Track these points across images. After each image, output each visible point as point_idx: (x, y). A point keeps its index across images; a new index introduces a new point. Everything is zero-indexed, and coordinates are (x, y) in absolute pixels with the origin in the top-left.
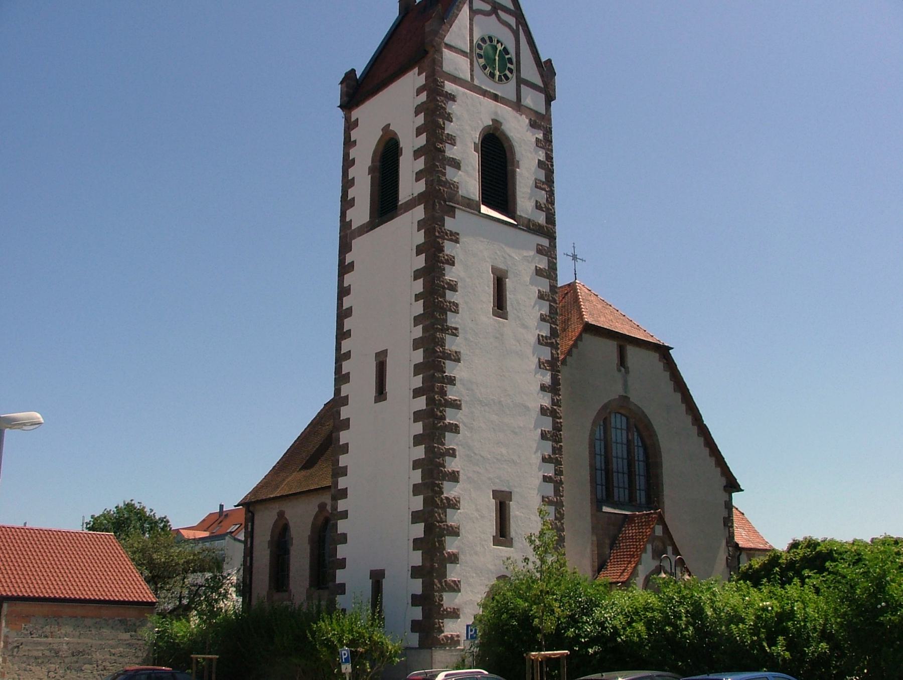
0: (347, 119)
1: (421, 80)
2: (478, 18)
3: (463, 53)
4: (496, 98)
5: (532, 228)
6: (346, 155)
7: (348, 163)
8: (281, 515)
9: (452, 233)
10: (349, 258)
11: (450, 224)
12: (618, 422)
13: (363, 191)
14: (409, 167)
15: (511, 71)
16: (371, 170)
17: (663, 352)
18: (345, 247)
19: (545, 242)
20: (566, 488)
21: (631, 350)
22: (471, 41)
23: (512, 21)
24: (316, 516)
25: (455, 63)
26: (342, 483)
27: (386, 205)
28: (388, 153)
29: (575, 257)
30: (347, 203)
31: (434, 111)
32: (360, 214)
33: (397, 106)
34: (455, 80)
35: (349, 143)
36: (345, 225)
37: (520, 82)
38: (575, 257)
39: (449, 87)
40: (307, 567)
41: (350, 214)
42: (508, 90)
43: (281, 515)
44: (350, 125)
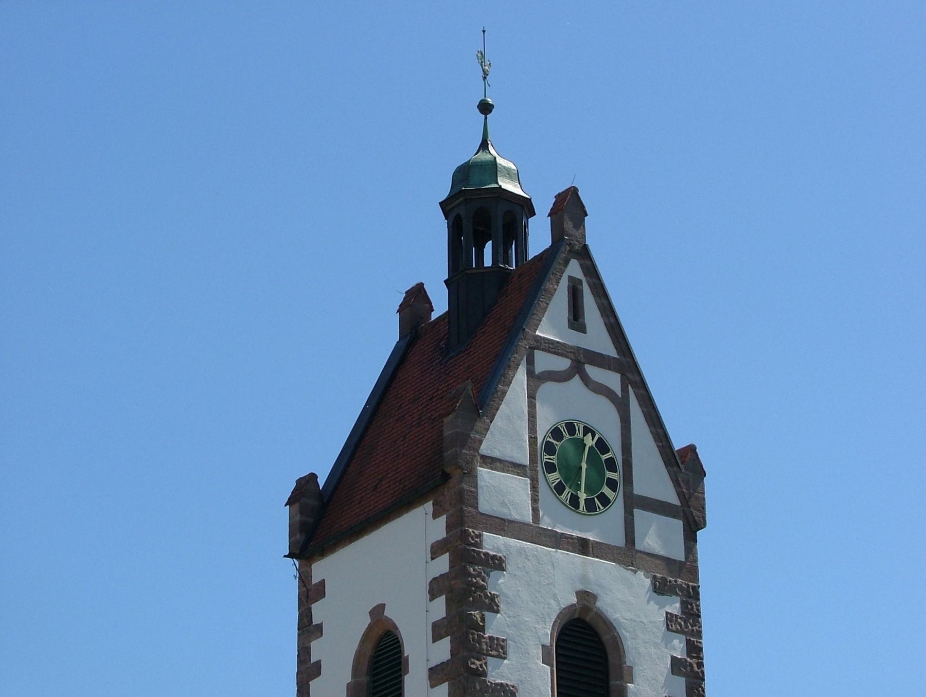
0: (304, 578)
1: (438, 529)
2: (547, 389)
4: (583, 547)
6: (304, 653)
15: (612, 485)
22: (533, 440)
23: (613, 380)
25: (502, 492)
31: (465, 590)
33: (392, 567)
34: (503, 526)
35: (308, 629)
37: (633, 503)
39: (492, 543)
42: (605, 527)
44: (310, 593)
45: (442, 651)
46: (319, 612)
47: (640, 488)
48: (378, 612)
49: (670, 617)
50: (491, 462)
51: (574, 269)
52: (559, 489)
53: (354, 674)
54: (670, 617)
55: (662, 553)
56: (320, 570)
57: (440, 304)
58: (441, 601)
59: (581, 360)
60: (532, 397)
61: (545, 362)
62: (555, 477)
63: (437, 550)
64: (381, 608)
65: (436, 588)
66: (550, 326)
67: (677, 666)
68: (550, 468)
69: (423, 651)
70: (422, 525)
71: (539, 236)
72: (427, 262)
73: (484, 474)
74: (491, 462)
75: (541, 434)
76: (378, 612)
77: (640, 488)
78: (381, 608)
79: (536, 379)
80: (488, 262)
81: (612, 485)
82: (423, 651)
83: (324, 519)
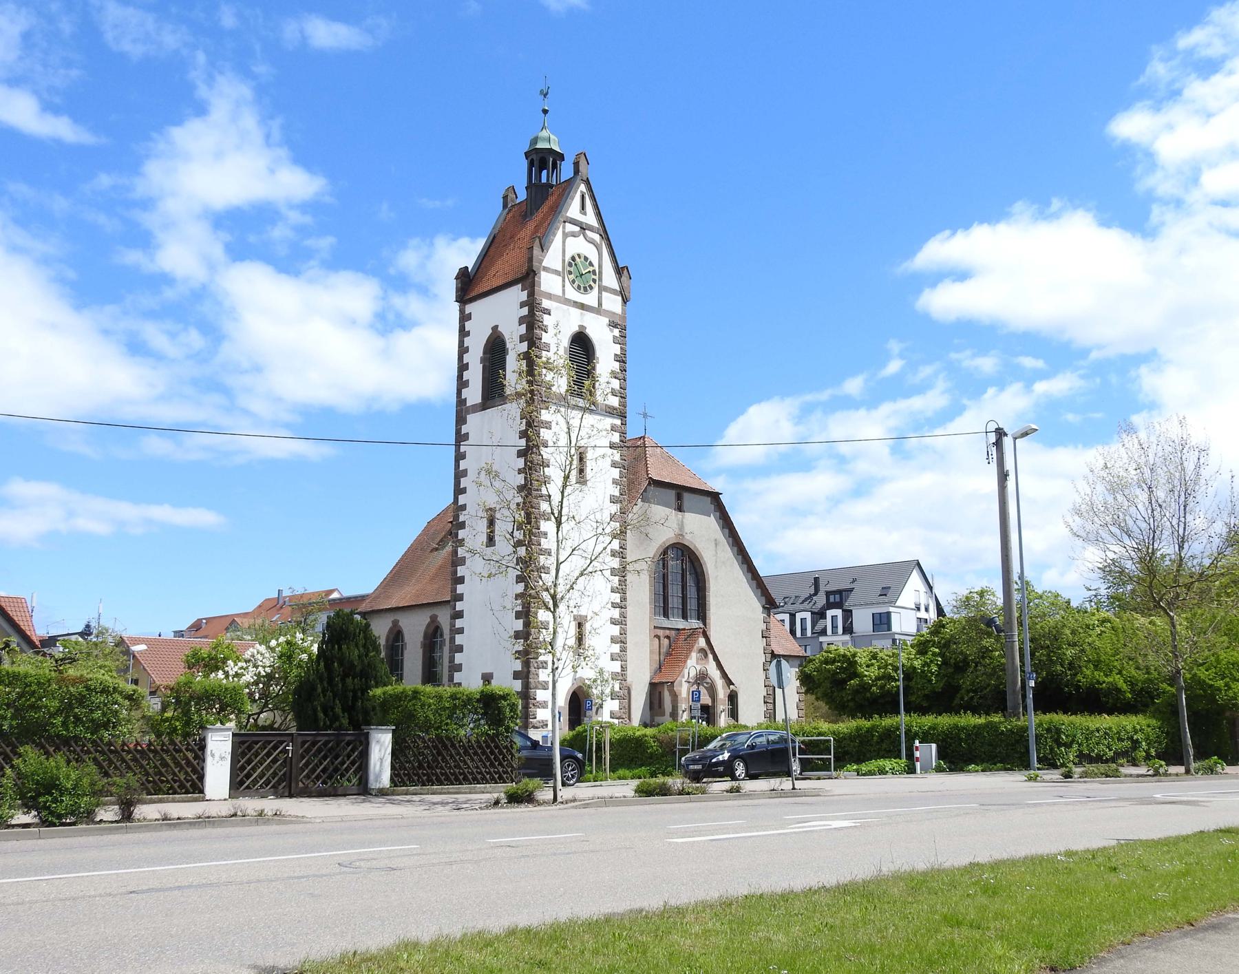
0: (462, 311)
1: (524, 296)
2: (570, 240)
3: (556, 272)
4: (582, 307)
5: (610, 412)
6: (461, 343)
7: (463, 350)
8: (395, 623)
9: (547, 422)
10: (464, 429)
11: (545, 415)
12: (674, 564)
13: (475, 375)
14: (513, 364)
15: (594, 281)
16: (483, 360)
17: (715, 497)
18: (461, 420)
19: (618, 422)
20: (630, 612)
21: (686, 496)
22: (564, 261)
23: (597, 237)
24: (429, 625)
25: (548, 283)
26: (459, 606)
27: (493, 392)
28: (495, 349)
29: (645, 416)
30: (462, 384)
31: (532, 322)
32: (474, 394)
33: (501, 311)
34: (550, 296)
35: (463, 333)
36: (461, 402)
37: (602, 289)
38: (645, 416)
39: (546, 303)
40: (420, 668)
41: (465, 393)
42: (591, 299)
43: (395, 623)
44: (464, 318)
45: (524, 347)
46: (468, 326)
47: (605, 283)
48: (495, 328)
49: (614, 337)
50: (546, 269)
51: (583, 188)
52: (573, 282)
53: (484, 353)
54: (614, 337)
55: (480, 244)
56: (469, 308)
57: (522, 195)
58: (524, 326)
59: (584, 228)
60: (564, 242)
61: (570, 228)
62: (572, 277)
63: (522, 305)
64: (497, 327)
65: (522, 320)
66: (573, 210)
67: (467, 350)
68: (570, 273)
69: (515, 348)
70: (517, 294)
71: (566, 171)
72: (518, 177)
73: (543, 274)
74: (546, 269)
75: (568, 258)
76: (495, 328)
77: (605, 283)
78: (497, 327)
79: (565, 235)
80: (544, 180)
81: (594, 281)
82: (515, 348)
83: (469, 287)
